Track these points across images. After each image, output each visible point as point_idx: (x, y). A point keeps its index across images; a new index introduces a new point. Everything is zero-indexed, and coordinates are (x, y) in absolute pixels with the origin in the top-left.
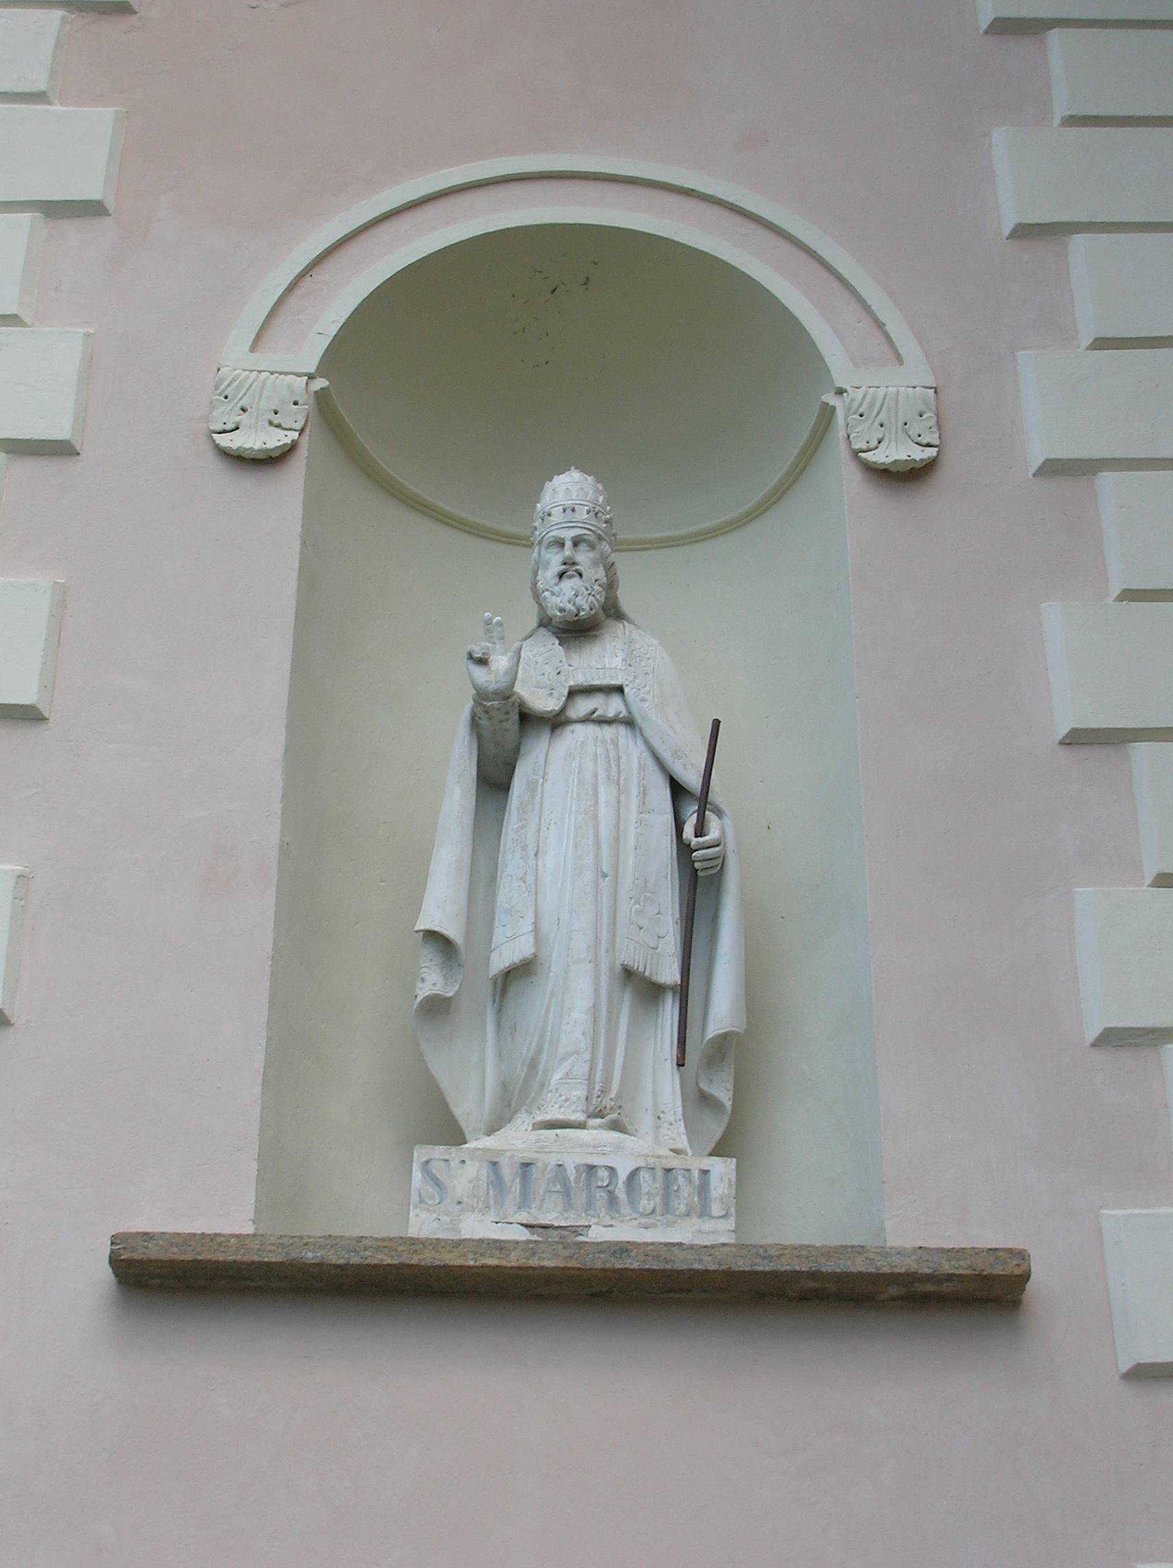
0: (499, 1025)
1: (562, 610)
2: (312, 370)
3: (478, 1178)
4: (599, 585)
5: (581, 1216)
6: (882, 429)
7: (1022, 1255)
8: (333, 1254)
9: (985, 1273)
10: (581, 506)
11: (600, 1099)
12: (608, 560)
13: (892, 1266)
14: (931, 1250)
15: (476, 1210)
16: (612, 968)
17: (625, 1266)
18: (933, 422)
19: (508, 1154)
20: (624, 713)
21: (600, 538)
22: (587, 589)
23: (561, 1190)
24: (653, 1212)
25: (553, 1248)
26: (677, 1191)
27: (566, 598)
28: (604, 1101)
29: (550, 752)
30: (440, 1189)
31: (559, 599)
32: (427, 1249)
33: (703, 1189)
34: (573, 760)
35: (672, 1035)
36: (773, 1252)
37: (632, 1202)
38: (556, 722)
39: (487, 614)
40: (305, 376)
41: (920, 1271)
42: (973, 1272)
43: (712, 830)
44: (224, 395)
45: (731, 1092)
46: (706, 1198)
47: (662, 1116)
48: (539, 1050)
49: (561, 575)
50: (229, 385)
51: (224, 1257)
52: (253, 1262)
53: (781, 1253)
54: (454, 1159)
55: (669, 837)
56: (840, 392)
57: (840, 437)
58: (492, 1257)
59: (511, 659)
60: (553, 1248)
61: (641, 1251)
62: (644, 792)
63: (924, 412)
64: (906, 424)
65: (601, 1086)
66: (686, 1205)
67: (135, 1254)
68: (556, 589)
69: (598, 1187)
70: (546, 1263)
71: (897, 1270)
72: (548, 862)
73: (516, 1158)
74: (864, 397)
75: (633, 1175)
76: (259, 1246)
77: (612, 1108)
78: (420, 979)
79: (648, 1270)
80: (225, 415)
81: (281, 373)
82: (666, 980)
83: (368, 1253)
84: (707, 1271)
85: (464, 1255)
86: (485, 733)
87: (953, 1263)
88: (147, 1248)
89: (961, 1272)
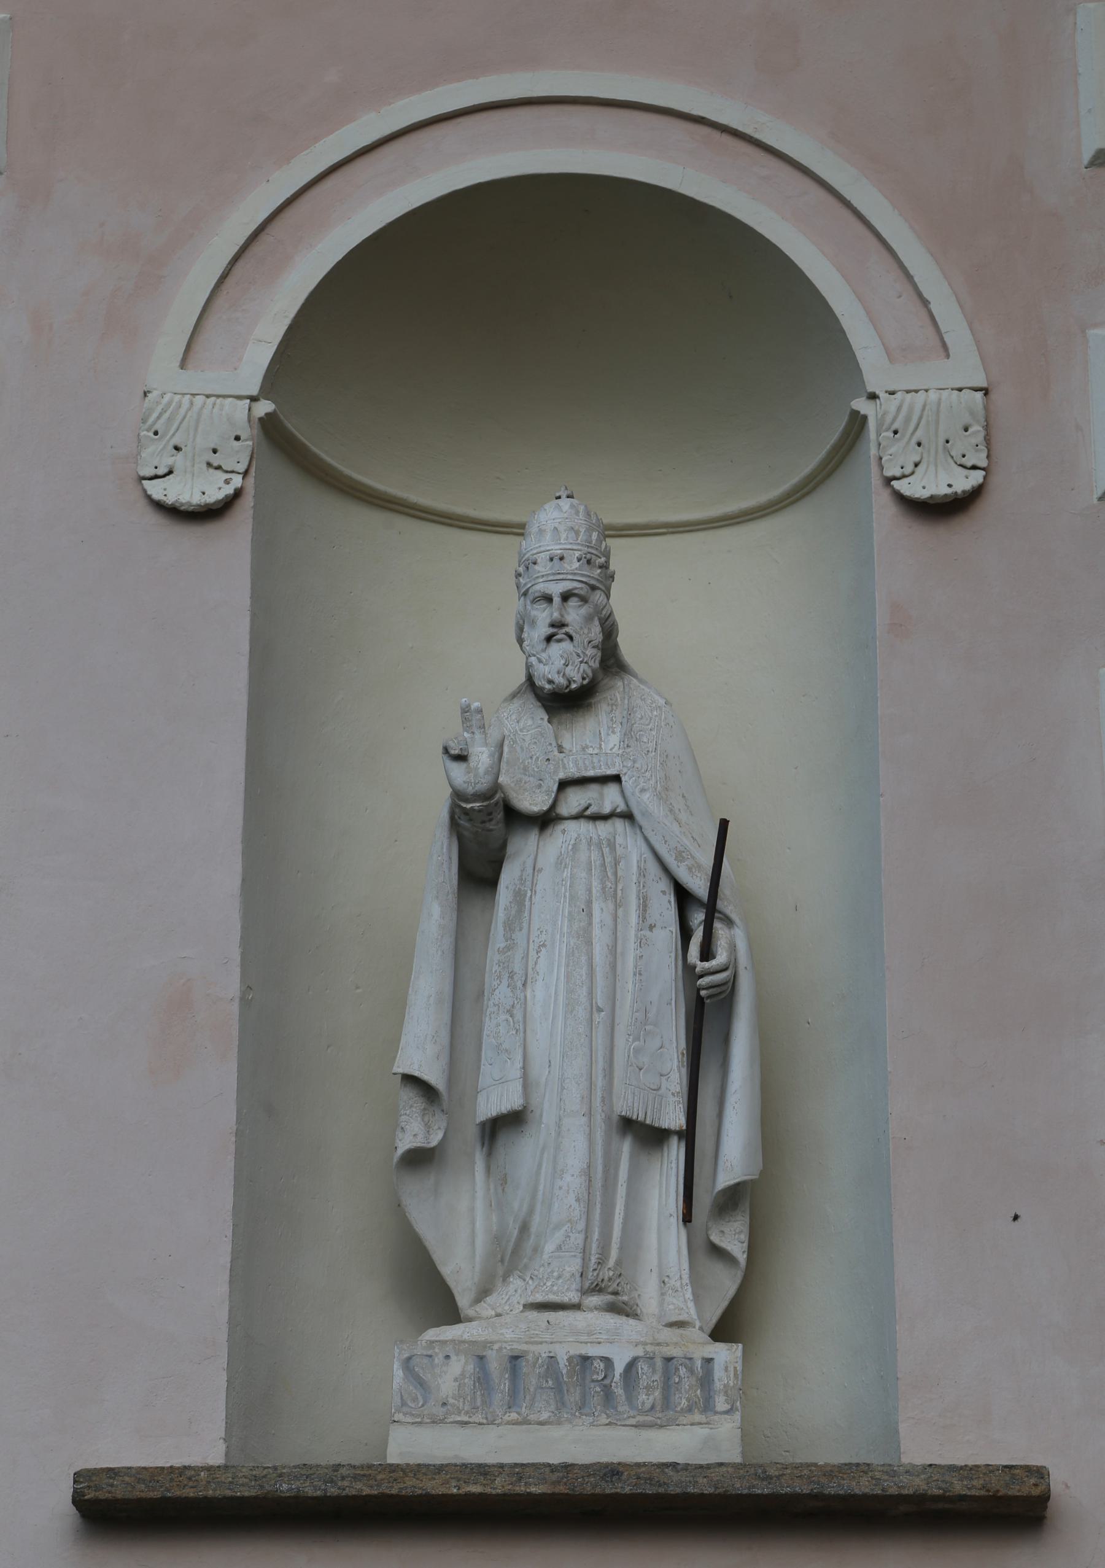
0: (488, 1170)
1: (550, 682)
2: (254, 392)
3: (463, 1374)
4: (593, 647)
5: (575, 1415)
6: (920, 449)
7: (1040, 1473)
8: (310, 1486)
9: (1000, 1494)
10: (572, 551)
11: (595, 1274)
12: (604, 612)
13: (899, 1487)
14: (944, 1467)
15: (463, 1412)
16: (608, 1119)
17: (616, 1490)
18: (980, 438)
19: (496, 1347)
20: (622, 808)
21: (593, 588)
22: (578, 655)
23: (553, 1387)
24: (653, 1407)
25: (540, 1471)
26: (678, 1383)
27: (555, 668)
28: (601, 1273)
29: (540, 855)
30: (424, 1389)
31: (547, 668)
32: (407, 1476)
33: (706, 1380)
34: (565, 867)
35: (677, 1184)
36: (772, 1472)
37: (630, 1398)
38: (546, 821)
39: (464, 700)
40: (248, 399)
41: (929, 1492)
42: (987, 1494)
43: (720, 950)
44: (153, 430)
45: (746, 1245)
46: (709, 1390)
47: (666, 1280)
48: (531, 1212)
49: (549, 639)
50: (159, 418)
51: (194, 1493)
52: (225, 1498)
53: (781, 1472)
54: (437, 1354)
55: (673, 955)
56: (873, 397)
57: (872, 457)
58: (476, 1484)
59: (491, 755)
60: (540, 1471)
61: (633, 1473)
62: (644, 906)
63: (970, 425)
64: (947, 442)
65: (598, 1258)
66: (688, 1400)
67: (100, 1492)
68: (544, 656)
69: (593, 1381)
70: (533, 1489)
71: (905, 1492)
72: (538, 993)
73: (505, 1350)
74: (899, 409)
75: (631, 1365)
76: (230, 1479)
77: (610, 1279)
78: (400, 1128)
79: (641, 1494)
80: (154, 458)
81: (218, 396)
82: (670, 1124)
83: (346, 1483)
84: (702, 1494)
85: (446, 1482)
86: (466, 833)
87: (965, 1483)
88: (112, 1485)
89: (973, 1492)
